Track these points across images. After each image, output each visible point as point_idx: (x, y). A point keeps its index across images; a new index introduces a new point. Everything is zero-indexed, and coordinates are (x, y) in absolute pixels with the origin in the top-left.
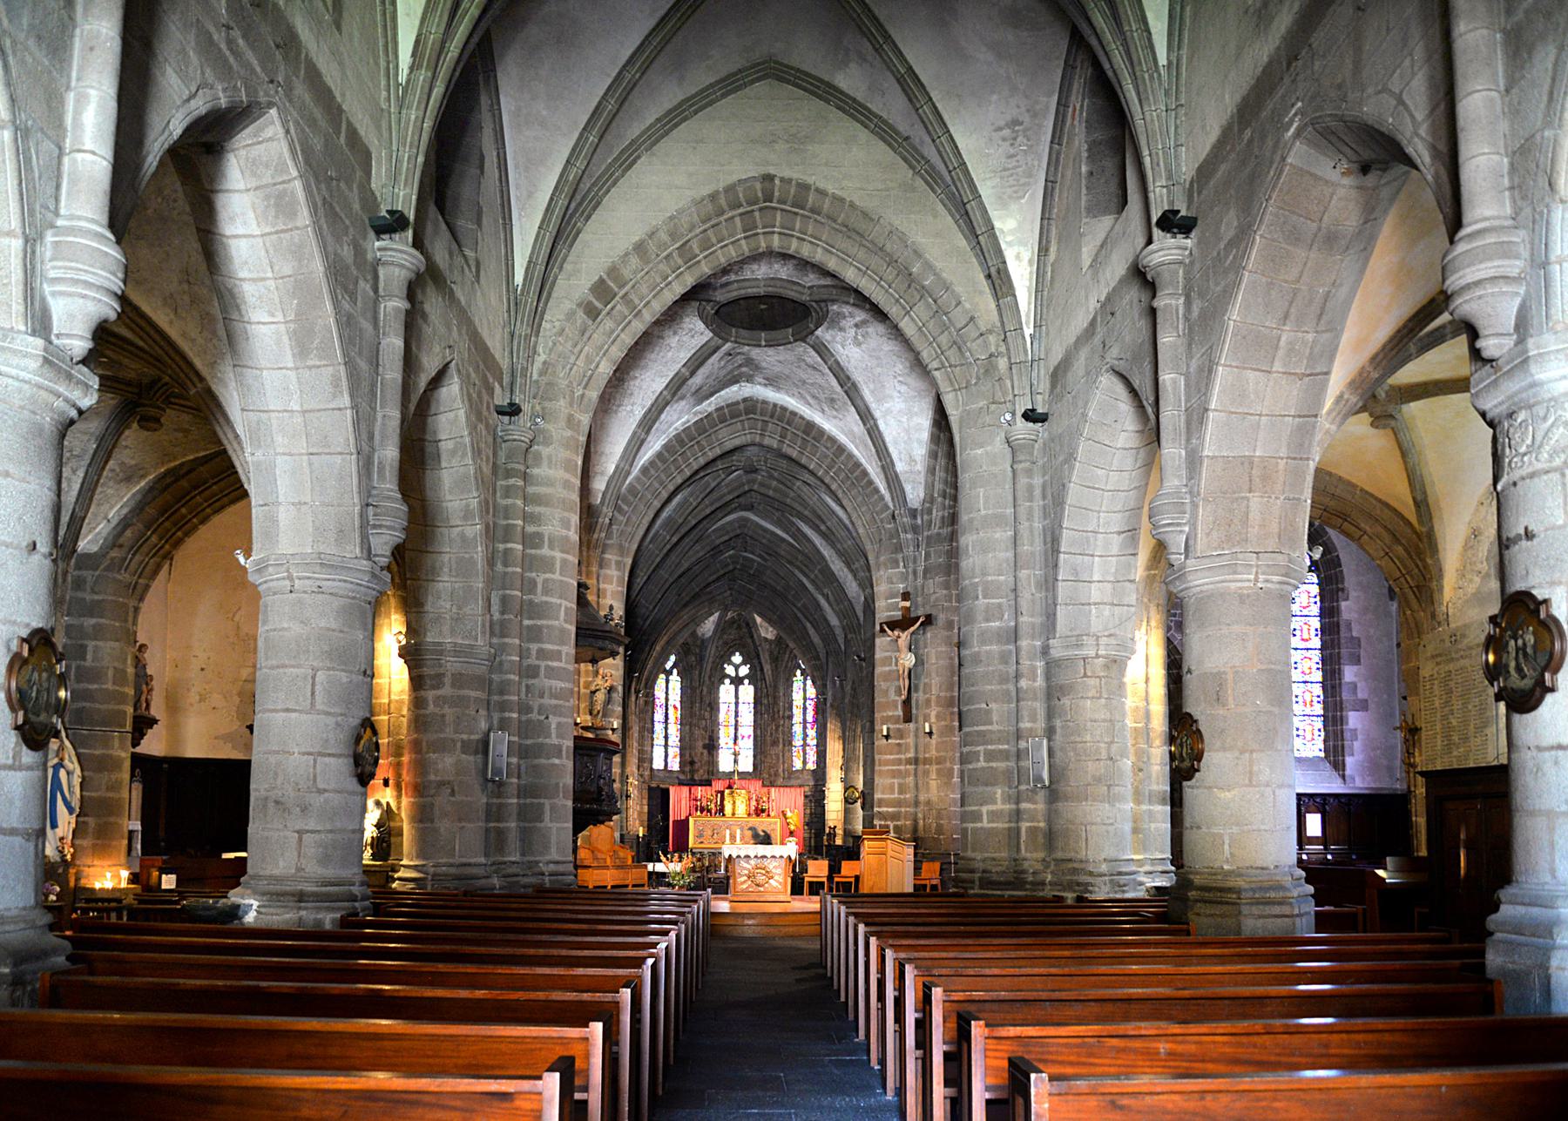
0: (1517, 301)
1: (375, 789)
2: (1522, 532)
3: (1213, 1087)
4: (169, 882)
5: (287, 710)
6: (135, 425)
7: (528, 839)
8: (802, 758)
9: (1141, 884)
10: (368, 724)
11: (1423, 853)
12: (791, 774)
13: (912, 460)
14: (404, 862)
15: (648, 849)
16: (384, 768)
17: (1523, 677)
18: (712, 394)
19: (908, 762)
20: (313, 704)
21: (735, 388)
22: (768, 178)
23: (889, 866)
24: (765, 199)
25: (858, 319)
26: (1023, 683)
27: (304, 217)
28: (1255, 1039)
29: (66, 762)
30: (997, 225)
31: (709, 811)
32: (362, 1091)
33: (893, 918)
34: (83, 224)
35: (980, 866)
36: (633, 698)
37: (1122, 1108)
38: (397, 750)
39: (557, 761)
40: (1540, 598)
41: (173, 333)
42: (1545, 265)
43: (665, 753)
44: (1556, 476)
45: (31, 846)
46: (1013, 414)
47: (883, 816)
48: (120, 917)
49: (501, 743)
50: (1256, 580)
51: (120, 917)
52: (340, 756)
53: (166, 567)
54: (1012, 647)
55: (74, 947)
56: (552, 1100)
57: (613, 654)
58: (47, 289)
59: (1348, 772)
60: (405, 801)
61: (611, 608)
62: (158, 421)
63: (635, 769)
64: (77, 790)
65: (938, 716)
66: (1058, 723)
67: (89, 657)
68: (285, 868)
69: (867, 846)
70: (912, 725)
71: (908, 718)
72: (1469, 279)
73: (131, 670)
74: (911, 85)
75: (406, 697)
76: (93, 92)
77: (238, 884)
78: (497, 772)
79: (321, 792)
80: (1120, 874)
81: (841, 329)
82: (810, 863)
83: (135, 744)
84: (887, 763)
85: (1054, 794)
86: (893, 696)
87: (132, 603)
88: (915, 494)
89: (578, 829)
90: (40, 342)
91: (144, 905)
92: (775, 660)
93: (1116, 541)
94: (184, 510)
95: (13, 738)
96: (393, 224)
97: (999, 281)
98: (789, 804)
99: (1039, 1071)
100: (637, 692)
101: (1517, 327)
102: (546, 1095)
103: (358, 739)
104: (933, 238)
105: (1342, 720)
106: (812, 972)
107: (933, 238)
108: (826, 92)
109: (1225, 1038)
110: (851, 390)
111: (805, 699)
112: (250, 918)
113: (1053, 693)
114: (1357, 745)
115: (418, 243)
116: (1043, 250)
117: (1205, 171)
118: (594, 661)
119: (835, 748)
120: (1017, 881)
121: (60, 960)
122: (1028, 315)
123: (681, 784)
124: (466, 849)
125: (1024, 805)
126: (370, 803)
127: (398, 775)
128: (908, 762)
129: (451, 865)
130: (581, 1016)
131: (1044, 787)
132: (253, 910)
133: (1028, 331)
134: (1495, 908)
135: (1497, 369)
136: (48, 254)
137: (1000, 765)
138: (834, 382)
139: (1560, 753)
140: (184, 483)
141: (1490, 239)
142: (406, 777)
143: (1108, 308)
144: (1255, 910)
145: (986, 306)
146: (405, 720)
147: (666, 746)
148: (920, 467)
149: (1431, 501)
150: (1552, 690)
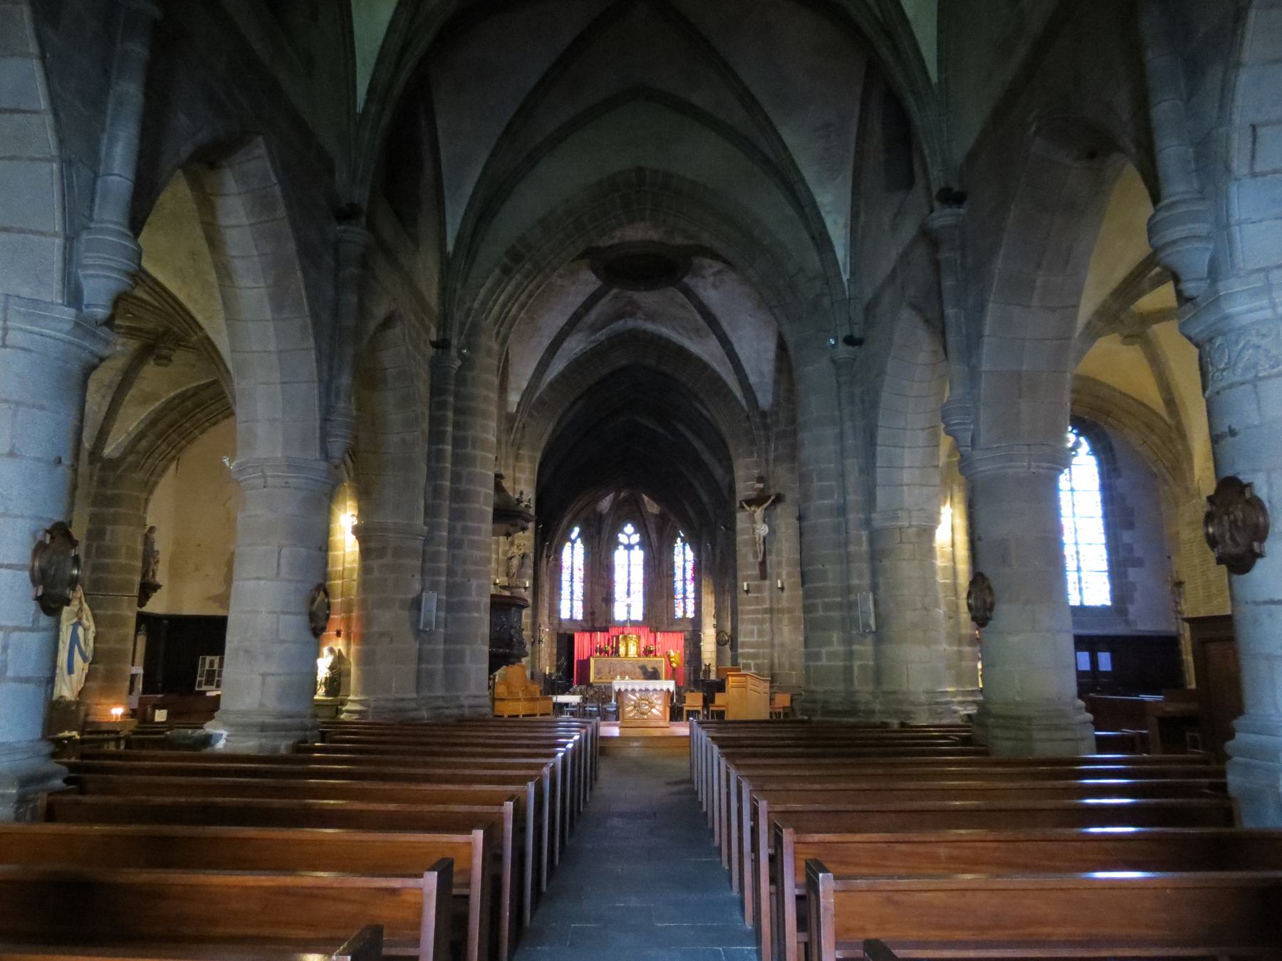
0: (1207, 256)
1: (329, 638)
2: (1226, 430)
3: (920, 887)
4: (161, 716)
5: (258, 578)
6: (152, 362)
7: (451, 678)
8: (684, 608)
9: (956, 712)
10: (324, 588)
11: (1193, 686)
12: (673, 621)
13: (762, 374)
14: (351, 697)
15: (553, 686)
16: (336, 617)
17: (1236, 543)
18: (604, 327)
19: (765, 611)
20: (278, 574)
21: (621, 322)
22: (640, 170)
23: (747, 698)
24: (637, 191)
25: (716, 269)
26: (852, 548)
27: (281, 211)
28: (1022, 845)
29: (84, 621)
30: (819, 199)
31: (607, 652)
32: (280, 887)
33: (741, 742)
34: (111, 226)
35: (820, 697)
36: (544, 561)
37: (896, 903)
38: (348, 607)
39: (476, 615)
40: (1245, 482)
41: (181, 297)
42: (1227, 226)
43: (571, 605)
44: (1249, 387)
45: (42, 690)
46: (836, 340)
47: (746, 656)
48: (118, 746)
49: (431, 601)
50: (1029, 467)
51: (118, 746)
52: (297, 614)
53: (173, 466)
54: (841, 519)
55: (71, 771)
56: (430, 895)
57: (524, 529)
58: (80, 272)
59: (1131, 617)
60: (353, 648)
61: (521, 493)
62: (169, 359)
63: (546, 619)
64: (91, 643)
65: (788, 574)
66: (881, 580)
67: (107, 538)
68: (247, 701)
69: (731, 681)
70: (767, 583)
71: (763, 575)
72: (1175, 236)
73: (140, 548)
74: (749, 102)
75: (356, 565)
76: (121, 133)
77: (212, 718)
78: (428, 624)
79: (283, 642)
80: (937, 703)
81: (704, 277)
82: (688, 695)
83: (141, 604)
84: (749, 612)
85: (879, 638)
86: (751, 559)
87: (144, 495)
88: (765, 399)
89: (493, 668)
90: (72, 311)
91: (142, 734)
92: (660, 530)
93: (922, 435)
94: (188, 425)
95: (33, 606)
96: (347, 214)
97: (822, 241)
98: (673, 649)
99: (825, 870)
100: (548, 557)
101: (1210, 273)
102: (426, 890)
103: (313, 601)
104: (767, 207)
105: (1125, 574)
106: (683, 787)
107: (767, 207)
108: (684, 108)
109: (995, 845)
110: (712, 322)
111: (685, 561)
112: (220, 745)
113: (876, 556)
114: (1137, 595)
115: (371, 227)
116: (855, 216)
117: (972, 157)
118: (508, 535)
119: (709, 600)
120: (852, 712)
121: (58, 783)
122: (845, 265)
123: (584, 631)
124: (401, 689)
125: (856, 647)
126: (325, 650)
127: (348, 627)
128: (765, 611)
129: (388, 700)
130: (464, 825)
131: (871, 632)
132: (222, 737)
133: (845, 277)
134: (1231, 736)
135: (1196, 305)
136: (82, 248)
137: (835, 614)
138: (698, 317)
139: (1273, 607)
140: (189, 404)
141: (1182, 209)
142: (355, 628)
143: (904, 258)
144: (1044, 735)
145: (813, 260)
146: (355, 584)
147: (572, 599)
148: (769, 379)
149: (1177, 401)
150: (1261, 555)
